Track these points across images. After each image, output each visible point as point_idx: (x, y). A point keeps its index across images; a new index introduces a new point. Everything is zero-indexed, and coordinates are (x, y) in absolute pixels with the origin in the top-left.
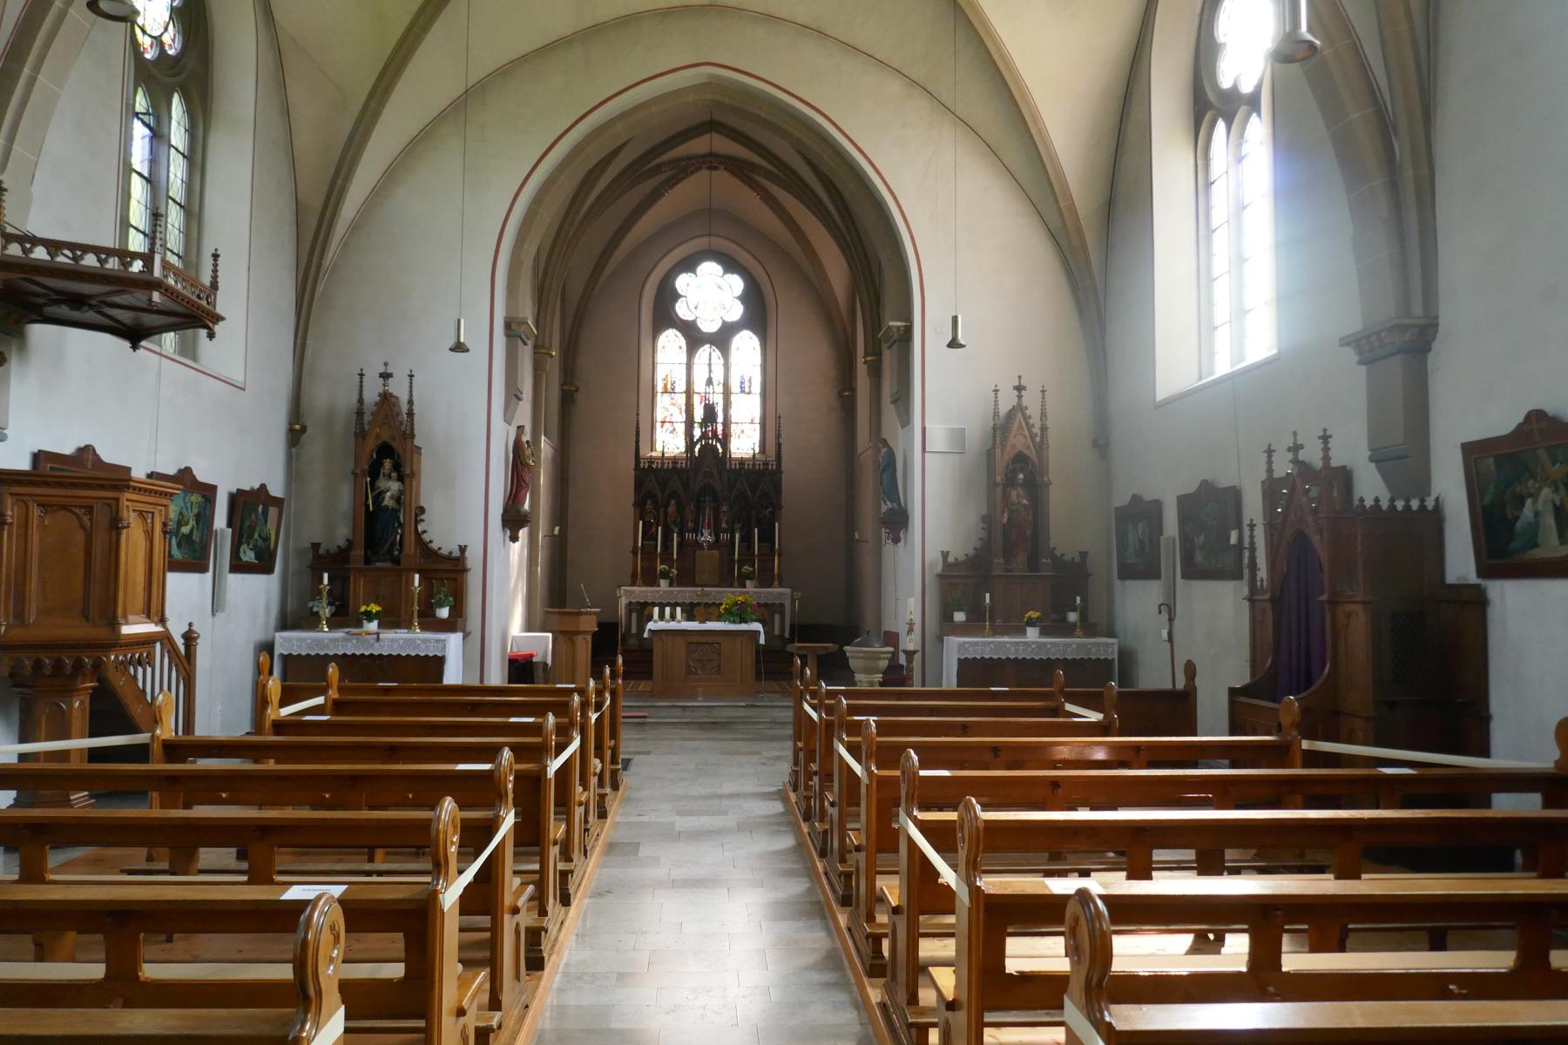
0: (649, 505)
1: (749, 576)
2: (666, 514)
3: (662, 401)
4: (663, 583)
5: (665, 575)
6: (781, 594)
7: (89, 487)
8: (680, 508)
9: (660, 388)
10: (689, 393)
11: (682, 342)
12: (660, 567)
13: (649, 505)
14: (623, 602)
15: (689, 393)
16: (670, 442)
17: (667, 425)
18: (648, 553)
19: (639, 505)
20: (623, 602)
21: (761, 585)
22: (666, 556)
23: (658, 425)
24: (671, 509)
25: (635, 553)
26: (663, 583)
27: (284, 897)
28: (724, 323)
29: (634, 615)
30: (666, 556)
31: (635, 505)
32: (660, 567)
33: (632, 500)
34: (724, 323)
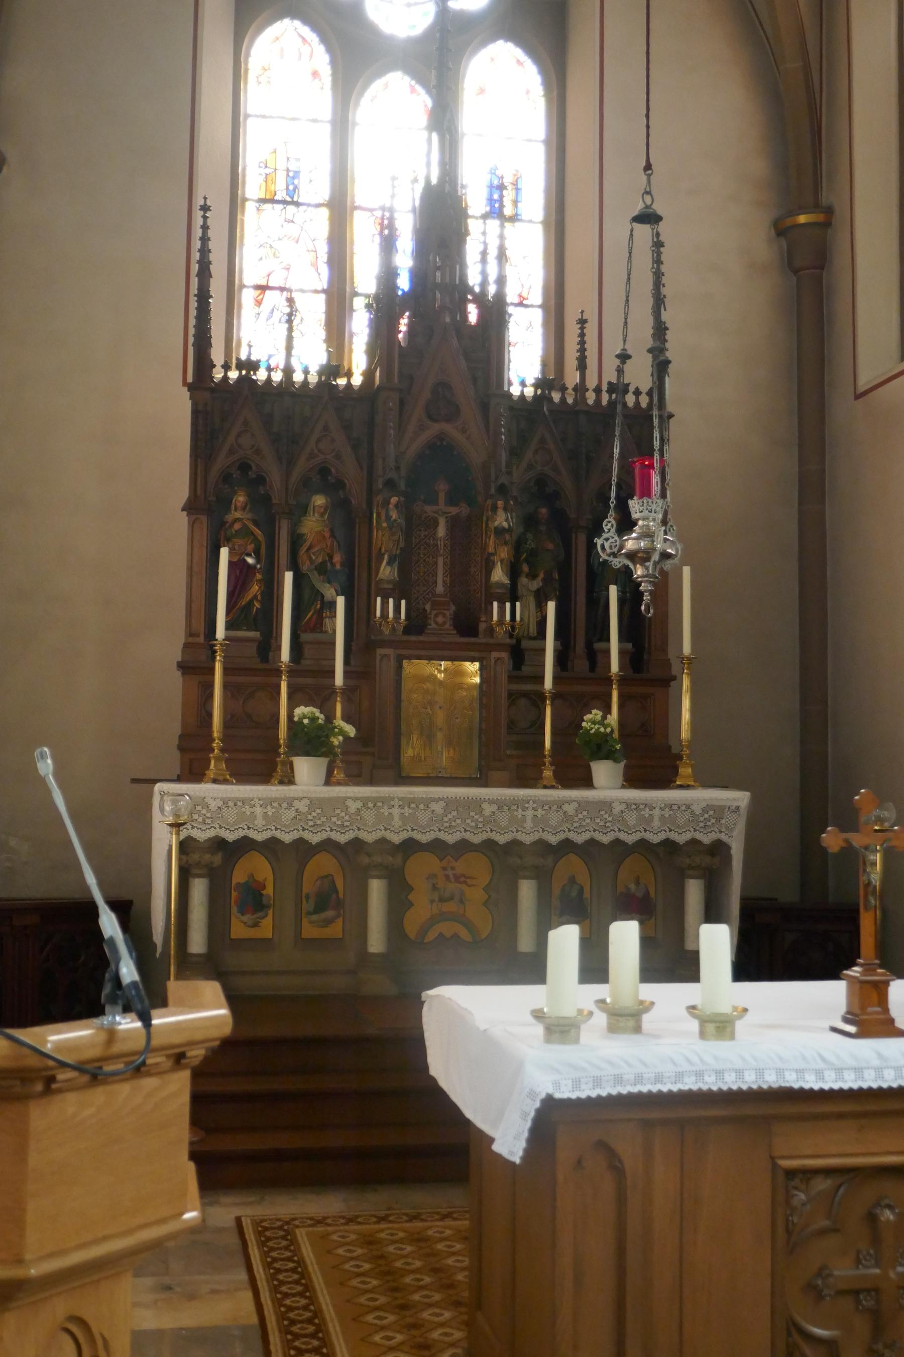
0: (240, 507)
1: (600, 748)
2: (296, 541)
3: (259, 227)
4: (307, 769)
5: (311, 741)
6: (718, 811)
7: (278, 1156)
8: (350, 520)
9: (253, 188)
10: (340, 209)
11: (321, 58)
12: (291, 711)
13: (240, 507)
14: (163, 843)
15: (340, 209)
16: (287, 325)
17: (273, 298)
18: (254, 669)
19: (207, 506)
20: (163, 843)
21: (632, 780)
22: (311, 682)
23: (247, 297)
24: (312, 525)
25: (195, 667)
26: (307, 769)
27: (685, 676)
28: (354, 311)
29: (199, 889)
30: (311, 682)
31: (190, 507)
32: (291, 711)
33: (183, 493)
34: (354, 311)
